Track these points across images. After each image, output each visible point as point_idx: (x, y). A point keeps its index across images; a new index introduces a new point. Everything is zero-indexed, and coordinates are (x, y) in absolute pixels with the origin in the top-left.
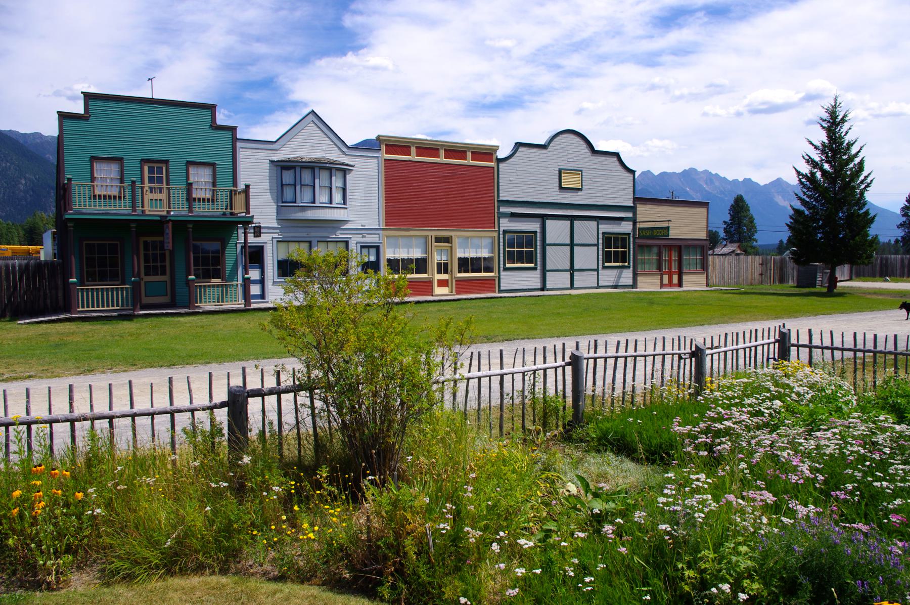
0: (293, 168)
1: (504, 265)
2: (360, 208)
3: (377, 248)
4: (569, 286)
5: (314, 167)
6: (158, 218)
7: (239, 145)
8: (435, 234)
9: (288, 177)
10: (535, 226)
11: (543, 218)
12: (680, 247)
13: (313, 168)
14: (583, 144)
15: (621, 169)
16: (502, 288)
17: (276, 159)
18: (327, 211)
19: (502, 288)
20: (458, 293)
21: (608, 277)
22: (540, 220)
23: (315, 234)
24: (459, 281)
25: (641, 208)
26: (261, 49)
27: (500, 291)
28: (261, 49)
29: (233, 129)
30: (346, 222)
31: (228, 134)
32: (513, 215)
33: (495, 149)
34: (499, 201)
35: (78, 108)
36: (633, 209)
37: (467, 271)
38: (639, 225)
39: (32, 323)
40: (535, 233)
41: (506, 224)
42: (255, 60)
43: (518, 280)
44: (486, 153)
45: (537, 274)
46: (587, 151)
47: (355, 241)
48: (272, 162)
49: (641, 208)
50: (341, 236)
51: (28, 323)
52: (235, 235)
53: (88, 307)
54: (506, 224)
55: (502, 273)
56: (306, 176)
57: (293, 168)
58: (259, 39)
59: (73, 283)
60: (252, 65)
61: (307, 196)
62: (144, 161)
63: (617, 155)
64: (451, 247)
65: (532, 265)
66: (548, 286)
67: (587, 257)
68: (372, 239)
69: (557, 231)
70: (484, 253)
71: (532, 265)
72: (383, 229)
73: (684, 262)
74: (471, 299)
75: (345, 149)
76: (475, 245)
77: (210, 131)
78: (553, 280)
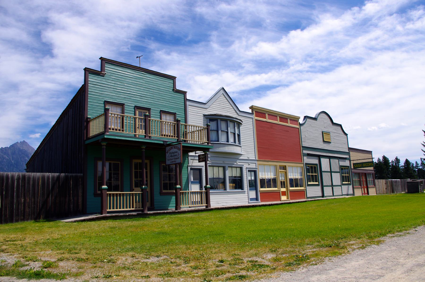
0: (216, 120)
1: (307, 183)
2: (246, 147)
3: (255, 172)
4: (332, 195)
5: (227, 119)
6: (162, 143)
7: (188, 103)
8: (278, 164)
9: (213, 125)
10: (315, 161)
11: (319, 157)
12: (365, 174)
13: (226, 121)
14: (329, 120)
15: (342, 133)
16: (308, 196)
17: (207, 114)
18: (235, 147)
19: (308, 196)
20: (291, 199)
21: (347, 189)
22: (317, 158)
23: (227, 161)
24: (292, 192)
25: (352, 153)
26: (42, 112)
27: (307, 198)
28: (42, 112)
29: (184, 93)
30: (241, 155)
31: (182, 96)
32: (309, 155)
33: (298, 118)
34: (303, 147)
35: (96, 66)
36: (348, 154)
37: (314, 182)
38: (352, 162)
39: (84, 220)
40: (317, 165)
41: (307, 160)
42: (40, 116)
43: (313, 191)
44: (295, 119)
45: (319, 188)
46: (330, 123)
47: (245, 166)
48: (205, 115)
49: (352, 153)
50: (239, 163)
51: (75, 222)
52: (186, 161)
53: (120, 208)
54: (307, 160)
55: (307, 187)
56: (223, 126)
57: (216, 120)
58: (42, 108)
59: (105, 189)
60: (39, 118)
61: (223, 139)
62: (136, 108)
63: (340, 126)
64: (286, 172)
65: (317, 183)
66: (325, 195)
67: (337, 178)
68: (253, 166)
69: (325, 162)
70: (298, 176)
71: (317, 183)
72: (257, 160)
73: (368, 182)
74: (298, 202)
75: (238, 112)
76: (294, 173)
77: (173, 93)
78: (328, 191)
